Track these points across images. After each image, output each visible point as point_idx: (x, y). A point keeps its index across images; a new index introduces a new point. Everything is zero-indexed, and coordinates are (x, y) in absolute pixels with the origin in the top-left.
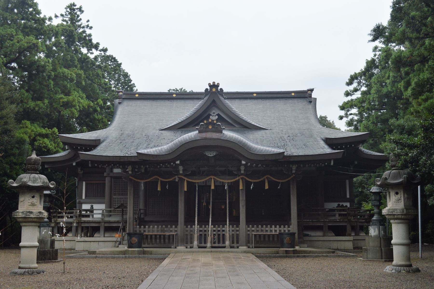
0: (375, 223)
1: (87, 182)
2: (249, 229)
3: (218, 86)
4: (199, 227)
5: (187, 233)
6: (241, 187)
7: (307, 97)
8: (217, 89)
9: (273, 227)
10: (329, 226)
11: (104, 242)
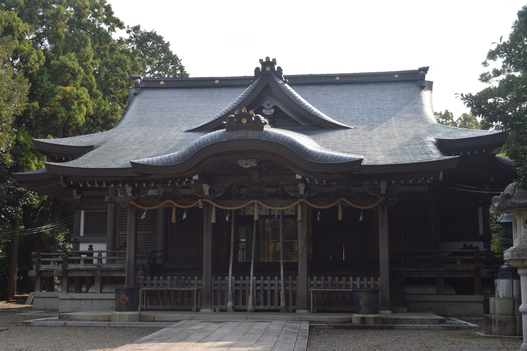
0: (506, 274)
1: (86, 211)
3: (274, 62)
4: (234, 279)
5: (216, 288)
7: (418, 80)
9: (350, 280)
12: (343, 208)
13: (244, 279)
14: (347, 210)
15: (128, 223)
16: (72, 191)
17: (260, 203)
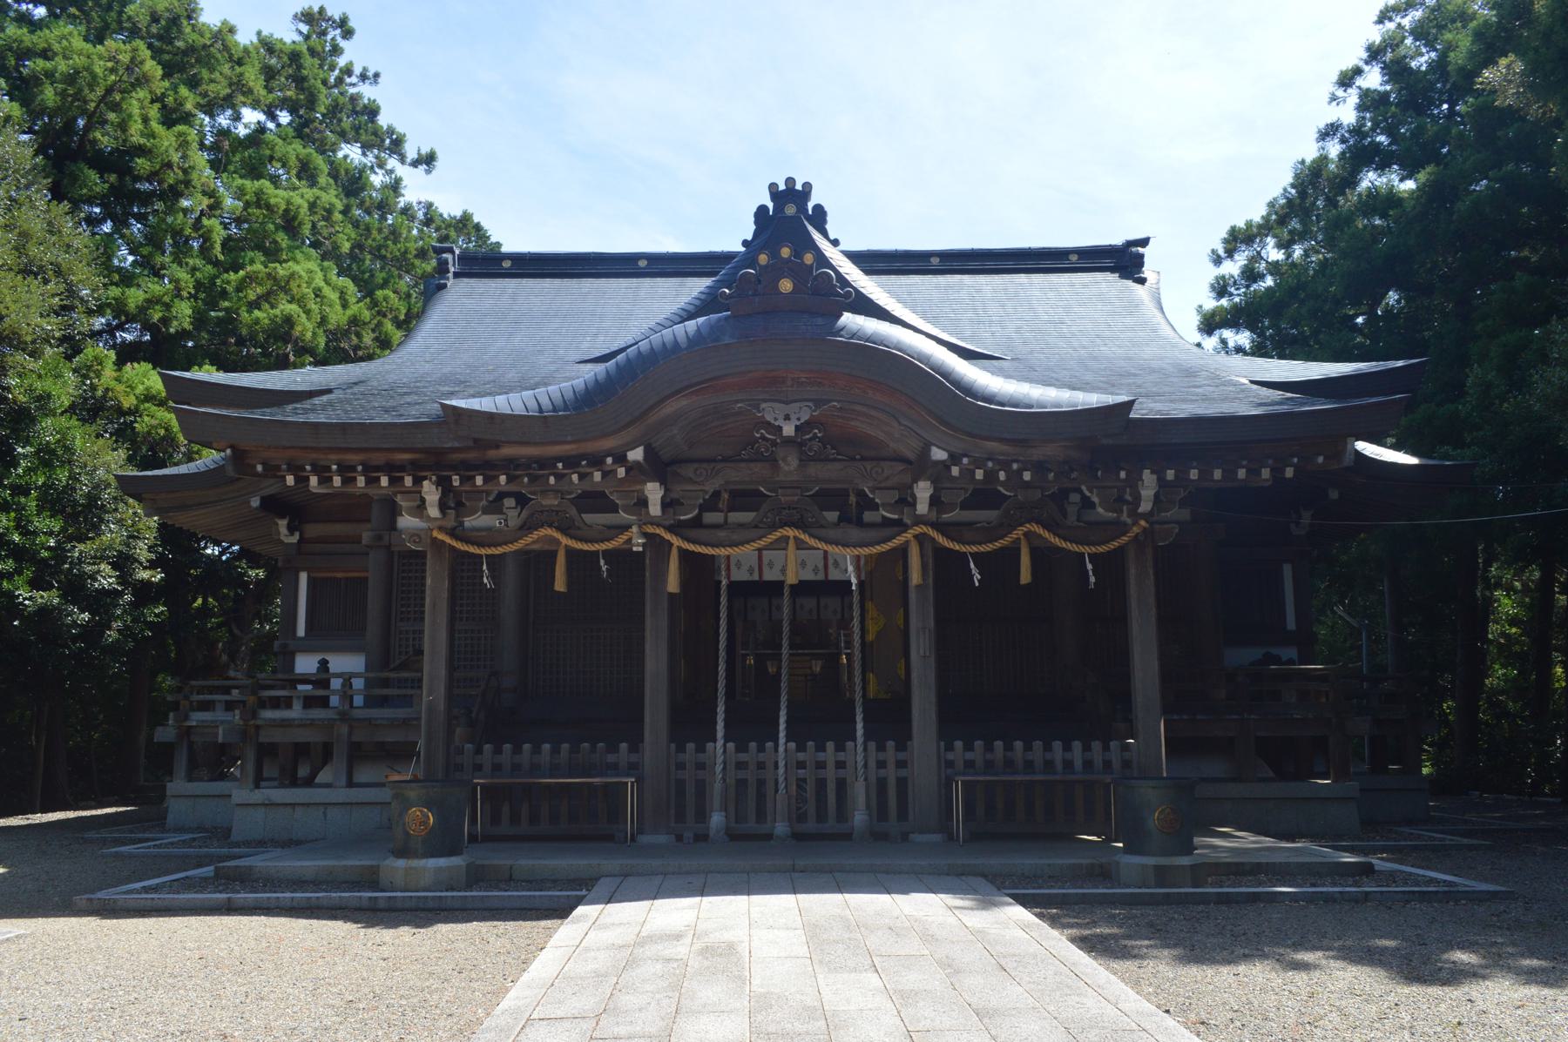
6: (915, 577)
12: (1034, 552)
13: (761, 749)
14: (1041, 555)
15: (428, 592)
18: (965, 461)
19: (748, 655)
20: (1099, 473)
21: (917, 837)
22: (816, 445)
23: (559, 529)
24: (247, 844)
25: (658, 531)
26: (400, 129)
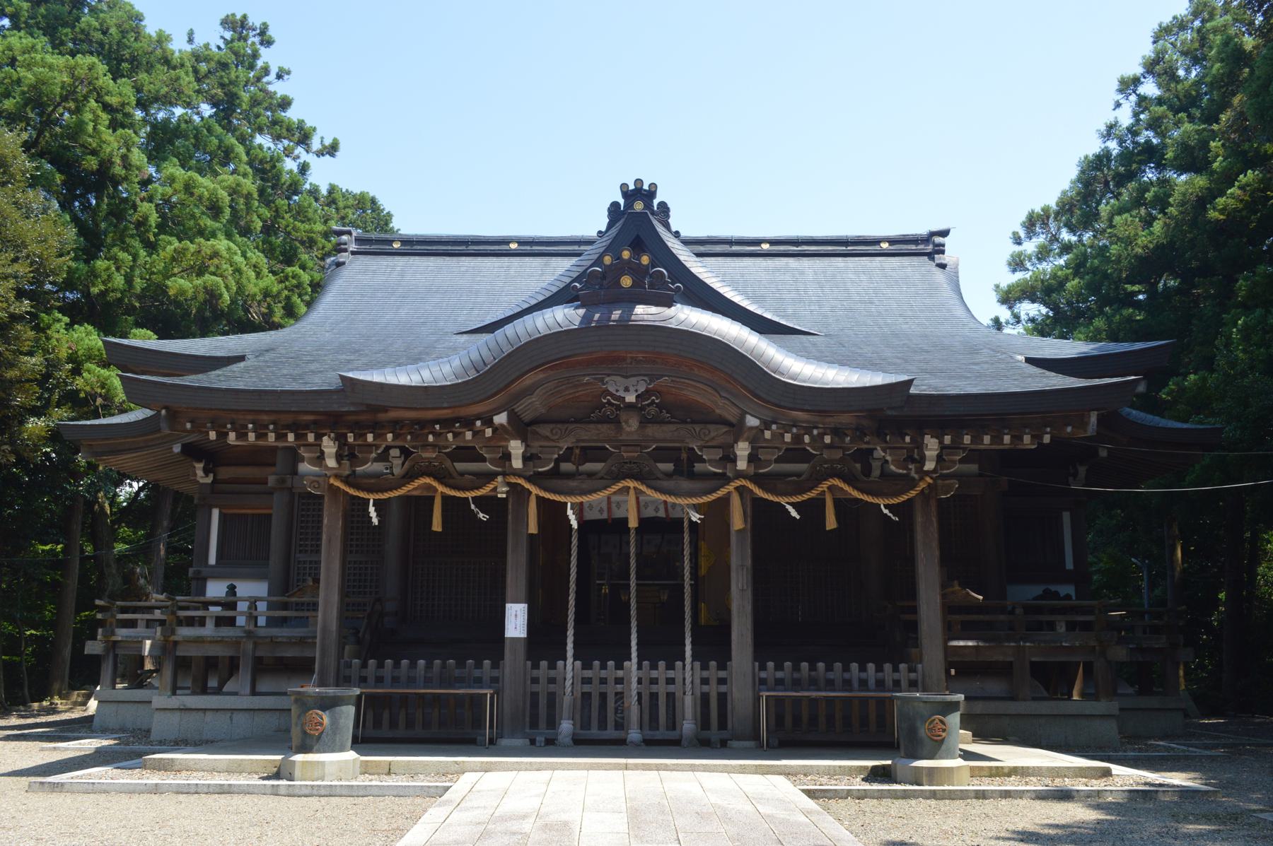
2: (763, 675)
3: (651, 194)
8: (649, 205)
10: (1032, 663)
11: (252, 712)
12: (838, 504)
14: (844, 506)
15: (325, 529)
16: (195, 467)
17: (643, 488)
18: (774, 427)
19: (603, 584)
20: (888, 438)
21: (735, 744)
22: (653, 410)
23: (436, 478)
24: (161, 743)
25: (521, 481)
26: (309, 123)
